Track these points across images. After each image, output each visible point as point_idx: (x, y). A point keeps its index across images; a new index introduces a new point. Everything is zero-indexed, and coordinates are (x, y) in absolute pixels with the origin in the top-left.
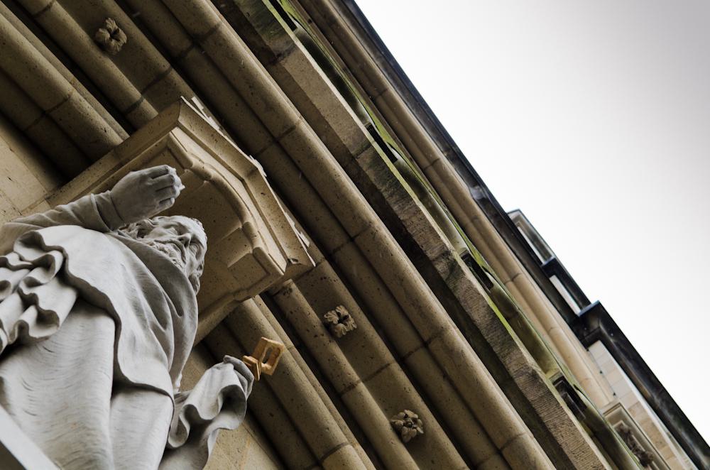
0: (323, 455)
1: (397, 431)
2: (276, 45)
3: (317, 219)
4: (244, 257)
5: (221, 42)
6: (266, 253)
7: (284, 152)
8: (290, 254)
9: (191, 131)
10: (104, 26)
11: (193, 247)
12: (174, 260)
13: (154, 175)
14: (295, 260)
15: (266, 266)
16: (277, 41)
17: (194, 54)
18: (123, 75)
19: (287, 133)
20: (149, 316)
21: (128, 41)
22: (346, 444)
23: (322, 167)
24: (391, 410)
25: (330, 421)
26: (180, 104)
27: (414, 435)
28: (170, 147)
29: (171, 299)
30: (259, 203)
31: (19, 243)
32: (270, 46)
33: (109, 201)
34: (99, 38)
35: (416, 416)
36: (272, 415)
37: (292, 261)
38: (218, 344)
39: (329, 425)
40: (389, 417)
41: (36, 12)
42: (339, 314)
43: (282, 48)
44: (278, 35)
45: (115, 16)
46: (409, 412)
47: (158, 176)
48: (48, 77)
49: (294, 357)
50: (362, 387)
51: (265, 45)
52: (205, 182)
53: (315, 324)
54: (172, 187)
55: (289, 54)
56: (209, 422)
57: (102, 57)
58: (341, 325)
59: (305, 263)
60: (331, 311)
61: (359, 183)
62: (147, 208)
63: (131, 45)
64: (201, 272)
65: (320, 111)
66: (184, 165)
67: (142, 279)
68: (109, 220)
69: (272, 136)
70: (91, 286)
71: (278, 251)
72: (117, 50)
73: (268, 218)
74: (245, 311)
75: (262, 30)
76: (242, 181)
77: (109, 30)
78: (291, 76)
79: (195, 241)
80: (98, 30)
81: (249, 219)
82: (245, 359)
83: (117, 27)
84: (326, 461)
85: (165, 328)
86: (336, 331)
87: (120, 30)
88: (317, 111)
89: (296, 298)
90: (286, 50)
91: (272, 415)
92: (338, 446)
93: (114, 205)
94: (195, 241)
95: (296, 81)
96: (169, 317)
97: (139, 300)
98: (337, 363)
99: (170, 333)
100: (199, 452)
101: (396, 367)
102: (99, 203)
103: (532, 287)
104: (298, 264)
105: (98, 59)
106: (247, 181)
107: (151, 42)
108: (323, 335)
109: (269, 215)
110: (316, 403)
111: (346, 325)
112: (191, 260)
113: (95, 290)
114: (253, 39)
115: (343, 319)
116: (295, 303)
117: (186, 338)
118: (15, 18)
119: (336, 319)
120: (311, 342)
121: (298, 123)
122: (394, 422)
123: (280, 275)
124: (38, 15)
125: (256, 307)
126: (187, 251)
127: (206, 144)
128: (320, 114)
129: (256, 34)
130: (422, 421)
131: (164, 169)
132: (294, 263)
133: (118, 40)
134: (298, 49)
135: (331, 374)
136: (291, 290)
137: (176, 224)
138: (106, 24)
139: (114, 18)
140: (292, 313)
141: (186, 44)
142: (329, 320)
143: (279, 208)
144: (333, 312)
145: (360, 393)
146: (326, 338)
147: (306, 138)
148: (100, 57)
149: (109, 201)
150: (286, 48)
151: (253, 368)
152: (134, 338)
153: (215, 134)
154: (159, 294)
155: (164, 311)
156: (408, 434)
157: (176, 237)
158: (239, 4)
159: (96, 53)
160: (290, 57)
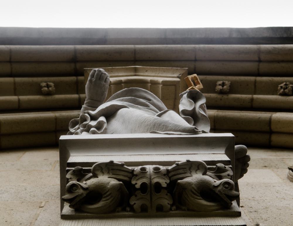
1: (284, 94)
4: (162, 89)
8: (176, 75)
10: (41, 87)
13: (93, 76)
14: (180, 75)
17: (78, 65)
21: (54, 84)
22: (272, 116)
24: (274, 92)
26: (86, 71)
27: (291, 89)
31: (71, 129)
33: (89, 100)
35: (284, 83)
37: (179, 76)
39: (259, 117)
40: (276, 94)
42: (220, 85)
46: (282, 85)
47: (94, 75)
50: (255, 96)
53: (216, 97)
56: (194, 109)
58: (225, 87)
59: (184, 72)
63: (56, 85)
69: (132, 61)
70: (105, 108)
73: (157, 75)
77: (45, 87)
83: (46, 83)
87: (49, 83)
96: (146, 103)
98: (238, 99)
99: (152, 107)
101: (259, 79)
102: (87, 105)
106: (137, 74)
111: (226, 85)
115: (223, 85)
117: (162, 108)
119: (220, 87)
121: (135, 47)
122: (280, 93)
123: (178, 82)
130: (288, 82)
131: (93, 71)
132: (180, 76)
133: (51, 86)
139: (42, 82)
141: (73, 65)
145: (257, 98)
146: (225, 97)
149: (89, 100)
154: (135, 99)
156: (289, 91)
159: (49, 98)
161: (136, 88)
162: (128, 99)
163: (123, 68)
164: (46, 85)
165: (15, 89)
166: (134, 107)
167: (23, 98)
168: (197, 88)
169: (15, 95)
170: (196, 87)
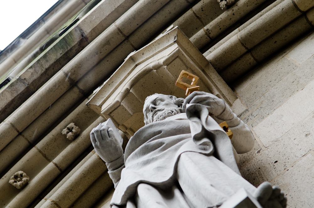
0: (299, 12)
2: (77, 38)
3: (170, 13)
5: (73, 71)
6: (167, 57)
7: (133, 33)
8: (172, 41)
9: (105, 97)
10: (65, 135)
11: (157, 104)
12: (161, 116)
14: (175, 38)
15: (173, 58)
16: (75, 37)
18: (91, 125)
19: (121, 32)
20: (155, 154)
21: (73, 122)
23: (140, 12)
25: (279, 8)
26: (90, 105)
28: (109, 113)
29: (148, 140)
30: (148, 56)
32: (78, 41)
33: (110, 164)
34: (72, 138)
36: (276, 42)
37: (175, 40)
38: (235, 74)
41: (59, 171)
43: (79, 34)
44: (72, 36)
45: (61, 129)
48: (88, 168)
49: (244, 28)
51: (77, 44)
52: (131, 91)
53: (227, 15)
54: (101, 131)
55: (81, 30)
57: (81, 136)
59: (176, 32)
60: (219, 5)
61: (16, 107)
62: (113, 144)
64: (174, 97)
65: (112, 11)
66: (118, 105)
67: (138, 155)
68: (120, 164)
69: (124, 40)
71: (170, 48)
72: (78, 129)
73: (154, 52)
74: (215, 59)
75: (69, 45)
76: (136, 66)
77: (68, 133)
78: (93, 29)
79: (154, 102)
80: (68, 139)
81: (151, 65)
82: (187, 95)
83: (66, 128)
84: (302, 10)
85: (164, 143)
86: (231, 2)
87: (68, 127)
88: (112, 13)
89: (212, 26)
90: (80, 31)
91: (276, 42)
92: (293, 2)
93: (112, 162)
94: (154, 102)
95: (96, 26)
97: (142, 161)
100: (217, 134)
102: (111, 169)
103: (16, 69)
104: (177, 36)
105: (83, 138)
106: (137, 63)
107: (74, 109)
108: (233, 10)
109: (153, 51)
110: (268, 16)
112: (164, 105)
113: (126, 192)
114: (74, 51)
116: (215, 27)
118: (61, 182)
120: (237, 17)
124: (60, 170)
125: (210, 54)
126: (158, 107)
127: (113, 88)
128: (114, 11)
129: (71, 49)
131: (92, 135)
132: (176, 39)
133: (73, 128)
134: (79, 25)
135: (256, 4)
136: (207, 30)
137: (146, 112)
138: (64, 134)
139: (62, 130)
140: (220, 29)
141: (76, 90)
142: (225, 6)
143: (150, 46)
144: (220, 4)
146: (235, 8)
147: (124, 21)
148: (82, 138)
149: (110, 164)
150: (79, 32)
151: (191, 91)
152: (158, 167)
153: (109, 83)
154: (146, 146)
155: (154, 144)
157: (151, 114)
158: (56, 59)
160: (83, 29)
161: (140, 131)
162: (140, 151)
163: (120, 69)
164: (68, 131)
165: (45, 156)
166: (150, 161)
167: (58, 159)
168: (193, 85)
169: (50, 161)
170: (192, 84)
